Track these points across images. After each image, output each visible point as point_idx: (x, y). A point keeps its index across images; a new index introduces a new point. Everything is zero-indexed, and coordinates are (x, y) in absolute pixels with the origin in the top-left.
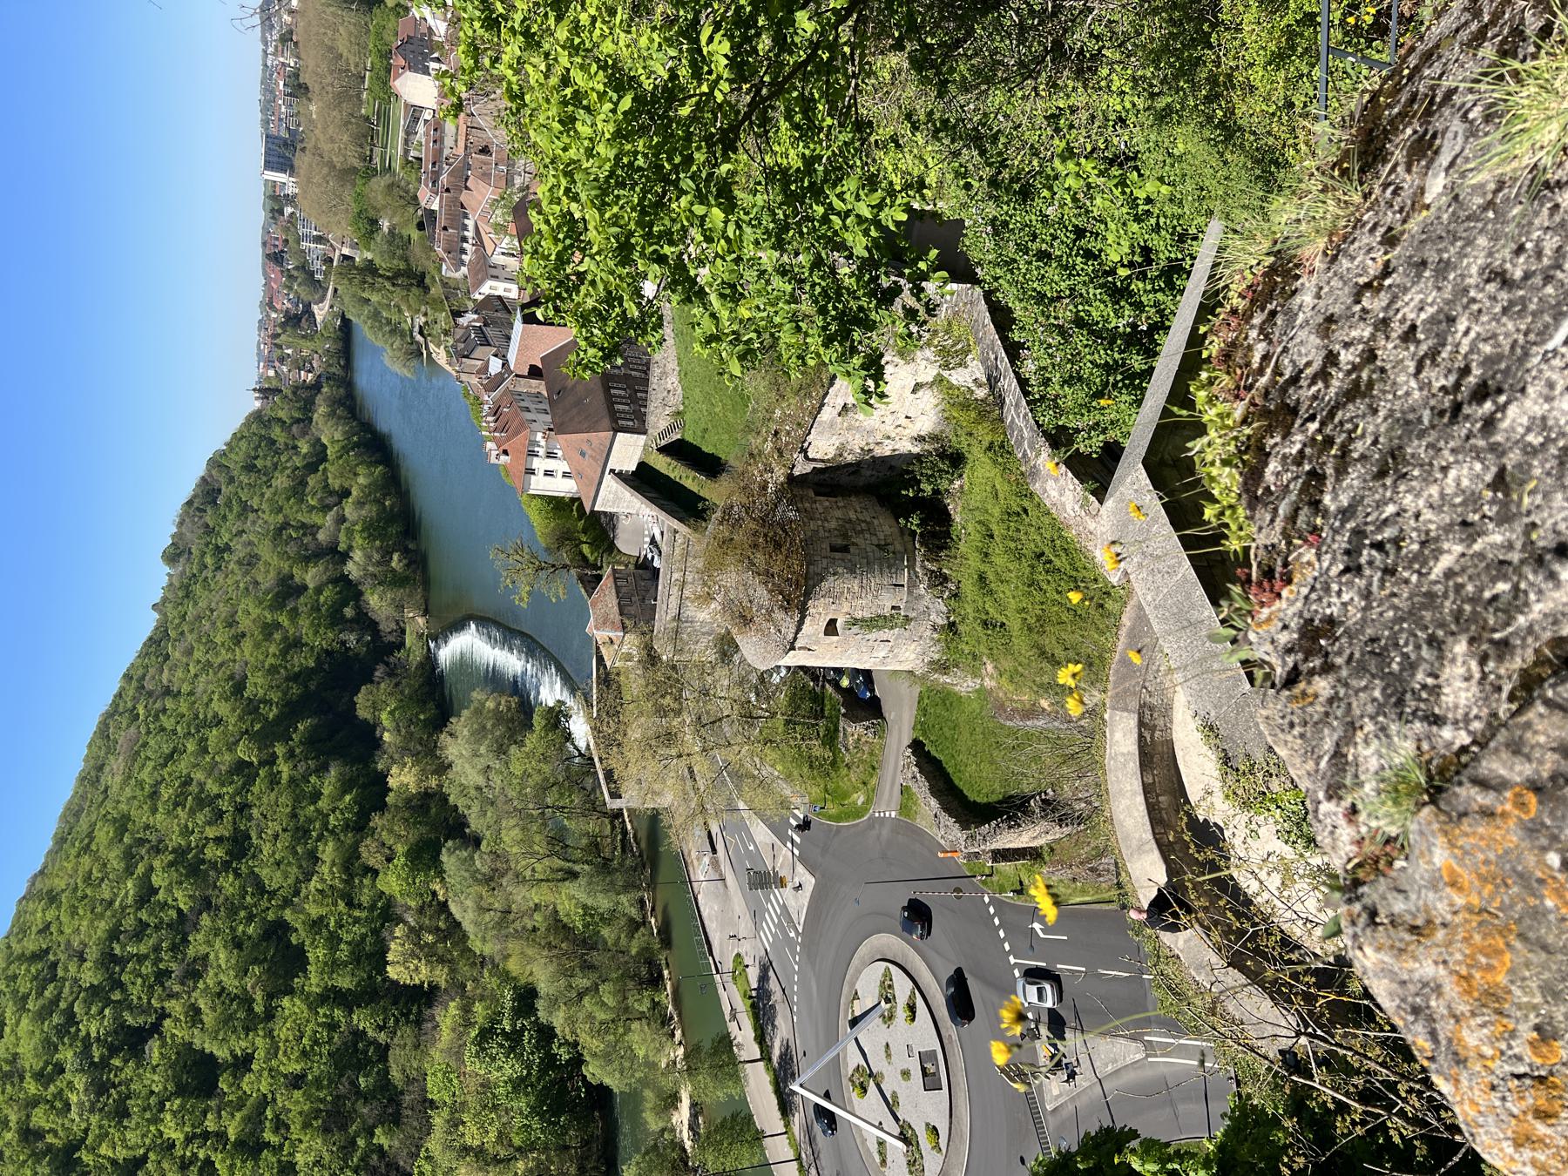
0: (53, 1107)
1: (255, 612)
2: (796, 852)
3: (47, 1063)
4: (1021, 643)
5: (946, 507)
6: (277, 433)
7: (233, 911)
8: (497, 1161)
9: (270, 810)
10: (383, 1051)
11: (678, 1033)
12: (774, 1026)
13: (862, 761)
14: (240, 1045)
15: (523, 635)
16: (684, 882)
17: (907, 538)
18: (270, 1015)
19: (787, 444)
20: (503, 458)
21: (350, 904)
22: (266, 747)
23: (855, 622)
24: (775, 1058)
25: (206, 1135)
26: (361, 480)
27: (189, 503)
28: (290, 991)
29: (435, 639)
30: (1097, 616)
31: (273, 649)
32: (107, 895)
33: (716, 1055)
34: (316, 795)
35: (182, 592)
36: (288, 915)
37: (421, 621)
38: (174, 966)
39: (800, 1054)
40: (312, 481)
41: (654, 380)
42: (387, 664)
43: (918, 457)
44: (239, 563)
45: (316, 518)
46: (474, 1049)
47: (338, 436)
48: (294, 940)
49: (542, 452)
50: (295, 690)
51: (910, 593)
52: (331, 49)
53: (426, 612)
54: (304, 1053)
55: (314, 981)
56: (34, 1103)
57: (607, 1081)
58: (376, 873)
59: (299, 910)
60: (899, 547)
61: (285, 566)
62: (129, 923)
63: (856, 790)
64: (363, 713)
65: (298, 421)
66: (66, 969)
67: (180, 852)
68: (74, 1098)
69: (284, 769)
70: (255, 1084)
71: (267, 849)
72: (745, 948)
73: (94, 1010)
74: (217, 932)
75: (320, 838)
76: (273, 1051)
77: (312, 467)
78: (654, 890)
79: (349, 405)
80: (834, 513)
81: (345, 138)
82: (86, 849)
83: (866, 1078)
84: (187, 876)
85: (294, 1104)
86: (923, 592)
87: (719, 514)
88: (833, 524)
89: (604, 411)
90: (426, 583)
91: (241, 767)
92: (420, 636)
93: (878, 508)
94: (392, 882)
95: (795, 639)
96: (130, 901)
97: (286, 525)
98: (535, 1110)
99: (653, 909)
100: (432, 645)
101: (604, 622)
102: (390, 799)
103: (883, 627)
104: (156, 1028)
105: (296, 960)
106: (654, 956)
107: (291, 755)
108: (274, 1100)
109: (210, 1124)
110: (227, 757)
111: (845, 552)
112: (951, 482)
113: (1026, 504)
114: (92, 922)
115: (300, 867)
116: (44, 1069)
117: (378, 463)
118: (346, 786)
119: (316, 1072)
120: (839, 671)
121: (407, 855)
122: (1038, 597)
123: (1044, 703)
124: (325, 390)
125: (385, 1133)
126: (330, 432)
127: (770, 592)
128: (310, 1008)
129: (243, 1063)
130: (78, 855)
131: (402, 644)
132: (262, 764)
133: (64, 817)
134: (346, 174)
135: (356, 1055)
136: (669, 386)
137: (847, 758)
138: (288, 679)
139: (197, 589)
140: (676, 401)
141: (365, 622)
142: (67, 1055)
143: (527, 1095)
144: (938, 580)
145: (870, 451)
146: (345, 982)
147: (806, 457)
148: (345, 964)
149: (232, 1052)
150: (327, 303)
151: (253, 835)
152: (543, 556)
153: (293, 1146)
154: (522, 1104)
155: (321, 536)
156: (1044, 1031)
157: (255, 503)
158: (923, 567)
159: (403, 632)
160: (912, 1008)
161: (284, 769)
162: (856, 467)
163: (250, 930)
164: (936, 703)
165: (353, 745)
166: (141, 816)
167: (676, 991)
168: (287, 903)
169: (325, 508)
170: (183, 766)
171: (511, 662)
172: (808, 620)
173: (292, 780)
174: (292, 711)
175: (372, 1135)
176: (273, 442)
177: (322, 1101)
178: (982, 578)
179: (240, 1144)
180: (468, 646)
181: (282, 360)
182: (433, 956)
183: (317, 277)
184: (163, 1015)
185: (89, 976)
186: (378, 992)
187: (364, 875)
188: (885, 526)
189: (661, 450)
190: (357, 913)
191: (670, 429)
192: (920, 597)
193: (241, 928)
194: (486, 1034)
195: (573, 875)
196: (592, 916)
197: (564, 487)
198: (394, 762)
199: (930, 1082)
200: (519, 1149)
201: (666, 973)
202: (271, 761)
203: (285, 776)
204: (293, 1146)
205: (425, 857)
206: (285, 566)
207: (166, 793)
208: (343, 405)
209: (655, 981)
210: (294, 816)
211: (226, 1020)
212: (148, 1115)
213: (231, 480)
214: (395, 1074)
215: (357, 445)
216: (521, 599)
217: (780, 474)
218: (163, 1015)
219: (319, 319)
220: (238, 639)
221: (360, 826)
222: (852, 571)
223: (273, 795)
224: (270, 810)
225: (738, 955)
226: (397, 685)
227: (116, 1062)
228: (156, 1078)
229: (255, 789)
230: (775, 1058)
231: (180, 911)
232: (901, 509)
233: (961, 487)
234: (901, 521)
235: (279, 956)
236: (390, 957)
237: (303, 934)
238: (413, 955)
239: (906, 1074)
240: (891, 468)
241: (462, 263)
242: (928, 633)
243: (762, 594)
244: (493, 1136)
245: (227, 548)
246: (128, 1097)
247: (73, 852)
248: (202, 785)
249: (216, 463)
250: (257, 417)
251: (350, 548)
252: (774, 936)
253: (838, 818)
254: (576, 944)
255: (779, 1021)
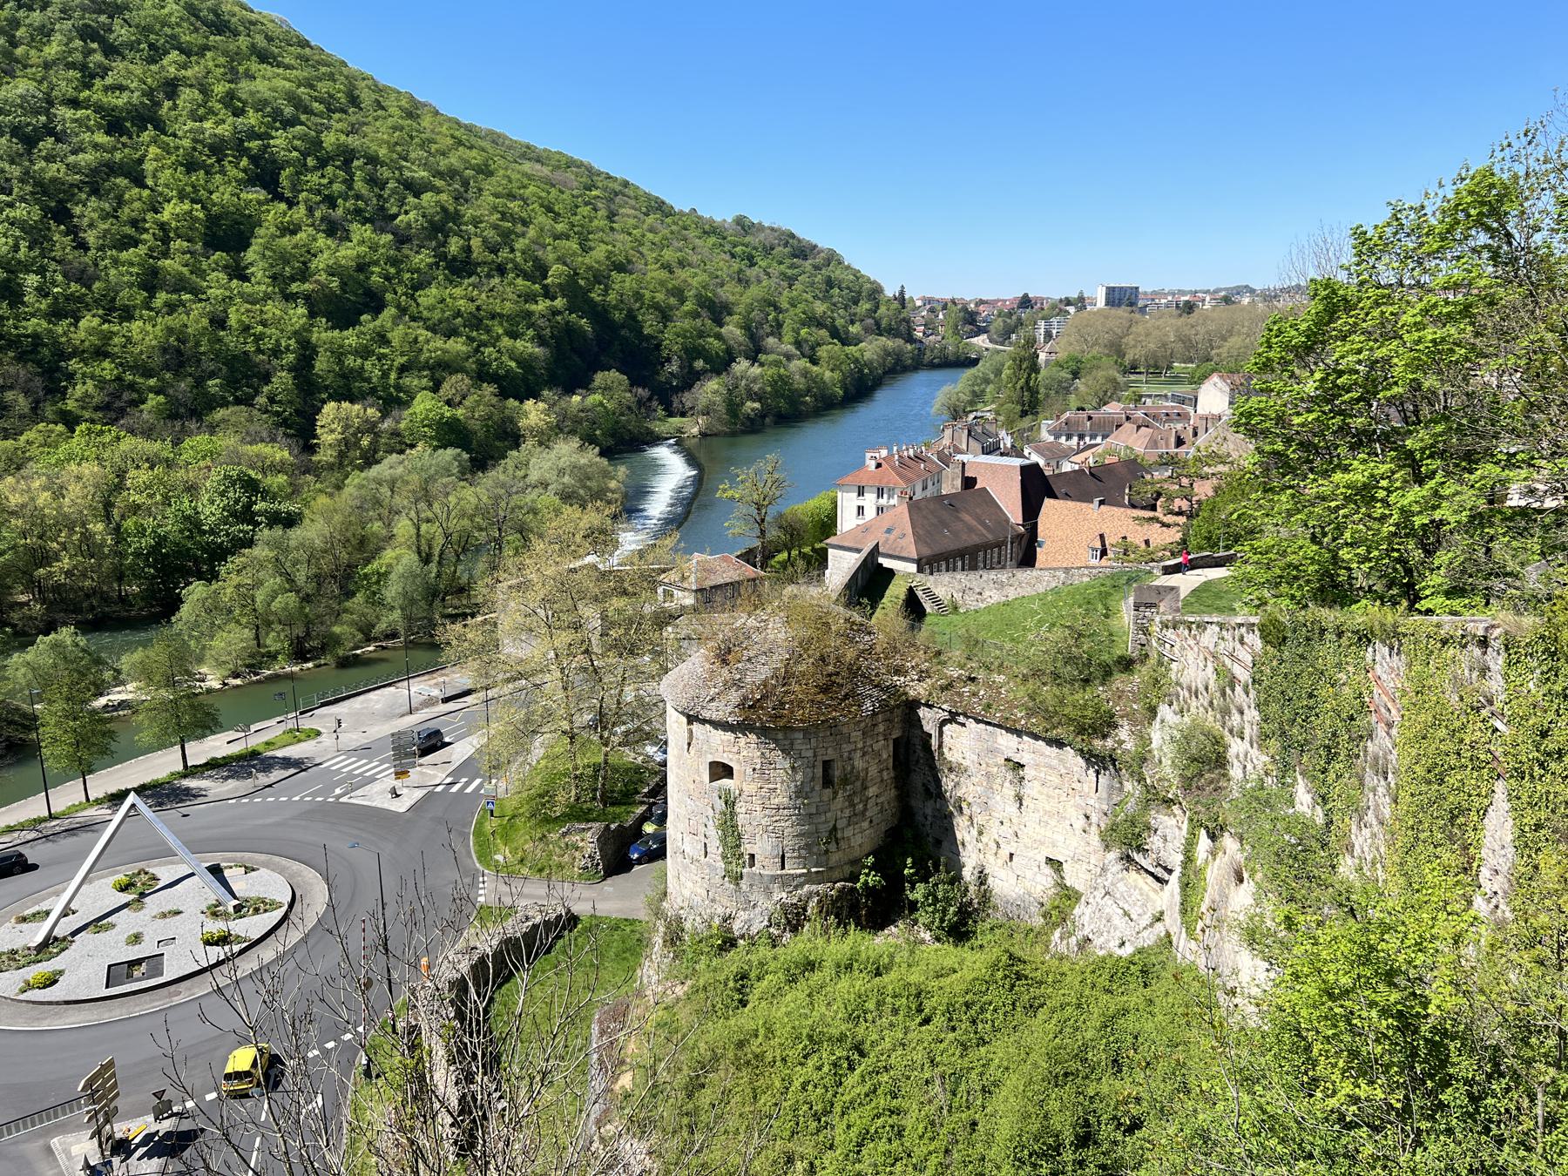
0: (199, 106)
1: (694, 282)
2: (439, 789)
3: (245, 103)
4: (718, 1032)
5: (893, 922)
6: (865, 306)
7: (394, 262)
8: (108, 505)
9: (504, 295)
10: (247, 401)
11: (238, 682)
12: (226, 778)
13: (550, 855)
14: (258, 271)
15: (687, 514)
16: (408, 673)
17: (848, 870)
18: (289, 298)
19: (960, 695)
20: (872, 464)
21: (403, 369)
22: (562, 290)
23: (730, 803)
24: (187, 783)
25: (166, 240)
26: (828, 374)
27: (792, 236)
28: (312, 314)
29: (677, 444)
30: (772, 1155)
31: (660, 297)
32: (413, 155)
33: (197, 717)
34: (514, 335)
35: (711, 230)
36: (389, 312)
37: (695, 430)
38: (340, 212)
39: (184, 811)
40: (824, 333)
41: (993, 575)
42: (650, 399)
43: (957, 879)
44: (740, 271)
45: (788, 336)
46: (234, 473)
47: (867, 355)
48: (364, 317)
49: (883, 501)
50: (617, 316)
51: (774, 878)
52: (1231, 332)
53: (704, 435)
54: (246, 329)
55: (324, 335)
56: (205, 91)
57: (185, 609)
58: (435, 389)
59: (396, 320)
60: (835, 858)
61: (740, 309)
62: (384, 173)
63: (514, 851)
64: (600, 378)
65: (878, 324)
66: (340, 120)
67: (457, 217)
68: (207, 125)
69: (542, 306)
70: (217, 284)
71: (458, 291)
72: (327, 740)
73: (296, 143)
74: (374, 248)
75: (471, 339)
76: (251, 300)
77: (835, 333)
78: (406, 648)
79: (897, 368)
80: (872, 762)
81: (1152, 346)
82: (460, 143)
83: (138, 889)
84: (431, 222)
85: (194, 318)
86: (776, 897)
87: (857, 618)
88: (859, 764)
89: (938, 549)
90: (733, 434)
91: (542, 270)
92: (680, 430)
93: (883, 828)
94: (424, 405)
95: (704, 721)
96: (407, 174)
97: (777, 308)
98: (161, 540)
99: (384, 648)
100: (672, 441)
101: (707, 570)
102: (512, 403)
103: (725, 845)
104: (279, 197)
105: (343, 317)
106: (325, 648)
107: (555, 312)
108: (201, 300)
109: (178, 244)
110: (551, 257)
111: (825, 779)
112: (928, 927)
113: (939, 1021)
114: (388, 143)
115: (440, 321)
116: (239, 100)
117: (845, 387)
118: (525, 362)
119: (226, 340)
120: (662, 819)
121: (455, 420)
122: (794, 1054)
123: (626, 1081)
124: (909, 347)
125: (159, 404)
126: (871, 349)
127: (765, 683)
128: (295, 333)
129: (239, 272)
130: (453, 136)
131: (671, 415)
132: (545, 287)
133: (491, 133)
134: (1117, 349)
135: (244, 377)
136: (987, 594)
137: (553, 836)
138: (630, 311)
139: (713, 240)
140: (971, 603)
141: (690, 379)
142: (252, 119)
143: (181, 531)
144: (794, 919)
145: (961, 809)
146: (321, 364)
147: (944, 723)
148: (340, 362)
149: (251, 264)
150: (990, 346)
151: (473, 279)
152: (772, 512)
153: (150, 319)
154: (171, 527)
155: (771, 341)
156: (166, 1125)
157: (798, 286)
158: (810, 896)
159: (683, 415)
160: (223, 940)
161: (542, 306)
162: (935, 792)
163: (375, 278)
164: (627, 942)
165: (568, 366)
166: (489, 185)
167: (291, 677)
168: (403, 311)
169: (798, 344)
170: (542, 219)
171: (658, 505)
172: (730, 736)
173: (529, 314)
174: (599, 314)
175: (158, 393)
176: (856, 303)
177: (198, 344)
178: (810, 966)
179: (155, 272)
180: (671, 471)
181: (932, 310)
182: (346, 446)
183: (1014, 336)
184: (291, 204)
185: (329, 140)
186: (310, 393)
187: (432, 378)
188: (861, 838)
189: (911, 591)
190: (393, 376)
191: (935, 600)
192: (769, 894)
193: (377, 269)
194: (251, 486)
195: (426, 560)
196: (378, 582)
197: (847, 521)
198: (552, 406)
199: (118, 972)
200: (118, 527)
201: (310, 665)
202: (548, 294)
203: (533, 307)
204: (150, 319)
205: (450, 433)
206: (740, 309)
207: (514, 206)
208: (896, 364)
209: (300, 654)
210: (493, 316)
211: (284, 258)
212: (189, 189)
213: (817, 268)
214: (220, 414)
215: (860, 371)
216: (725, 490)
217: (918, 690)
218: (291, 204)
219: (974, 340)
220: (667, 267)
221: (483, 375)
222: (799, 793)
223: (511, 296)
224: (504, 295)
225: (318, 734)
226: (629, 408)
227: (244, 162)
228: (226, 196)
229: (519, 281)
230: (187, 783)
231: (395, 216)
232: (886, 859)
233: (923, 942)
234: (871, 859)
235: (350, 302)
236: (345, 405)
237: (371, 326)
238: (346, 427)
239: (136, 939)
240: (938, 843)
241: (1057, 437)
242: (720, 911)
243: (760, 673)
244: (135, 498)
245: (752, 265)
246: (207, 173)
247: (457, 134)
248: (523, 235)
249: (832, 258)
250: (876, 292)
251: (762, 365)
252: (338, 771)
253: (479, 833)
254: (347, 571)
255: (232, 783)
